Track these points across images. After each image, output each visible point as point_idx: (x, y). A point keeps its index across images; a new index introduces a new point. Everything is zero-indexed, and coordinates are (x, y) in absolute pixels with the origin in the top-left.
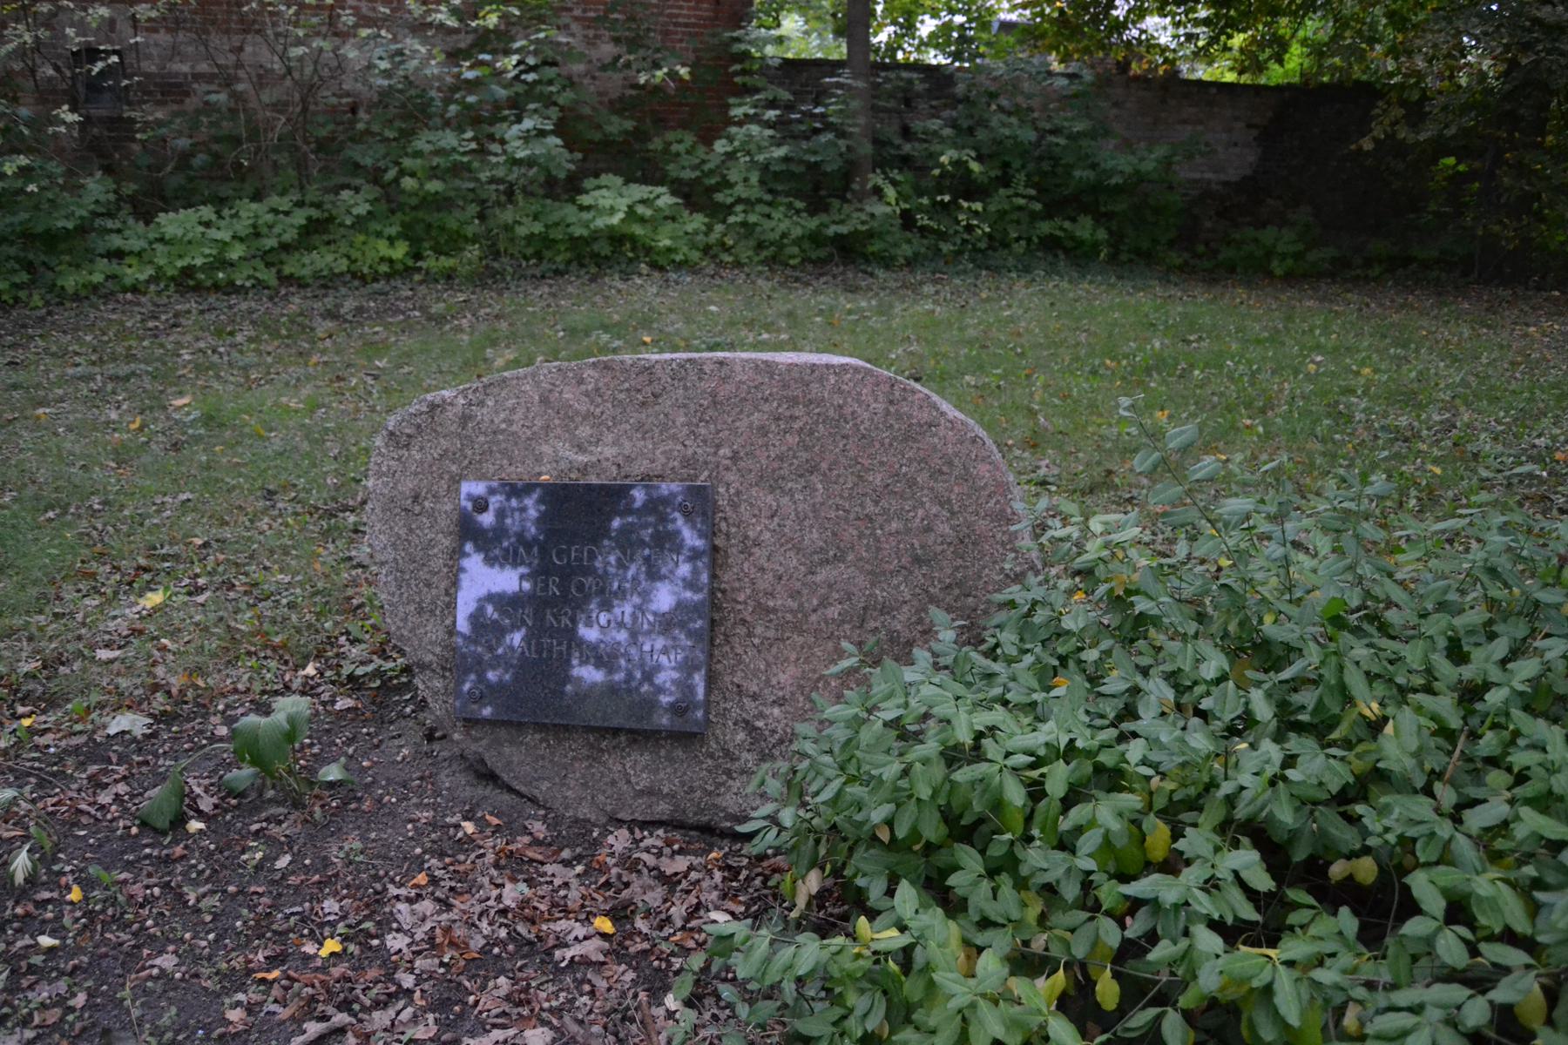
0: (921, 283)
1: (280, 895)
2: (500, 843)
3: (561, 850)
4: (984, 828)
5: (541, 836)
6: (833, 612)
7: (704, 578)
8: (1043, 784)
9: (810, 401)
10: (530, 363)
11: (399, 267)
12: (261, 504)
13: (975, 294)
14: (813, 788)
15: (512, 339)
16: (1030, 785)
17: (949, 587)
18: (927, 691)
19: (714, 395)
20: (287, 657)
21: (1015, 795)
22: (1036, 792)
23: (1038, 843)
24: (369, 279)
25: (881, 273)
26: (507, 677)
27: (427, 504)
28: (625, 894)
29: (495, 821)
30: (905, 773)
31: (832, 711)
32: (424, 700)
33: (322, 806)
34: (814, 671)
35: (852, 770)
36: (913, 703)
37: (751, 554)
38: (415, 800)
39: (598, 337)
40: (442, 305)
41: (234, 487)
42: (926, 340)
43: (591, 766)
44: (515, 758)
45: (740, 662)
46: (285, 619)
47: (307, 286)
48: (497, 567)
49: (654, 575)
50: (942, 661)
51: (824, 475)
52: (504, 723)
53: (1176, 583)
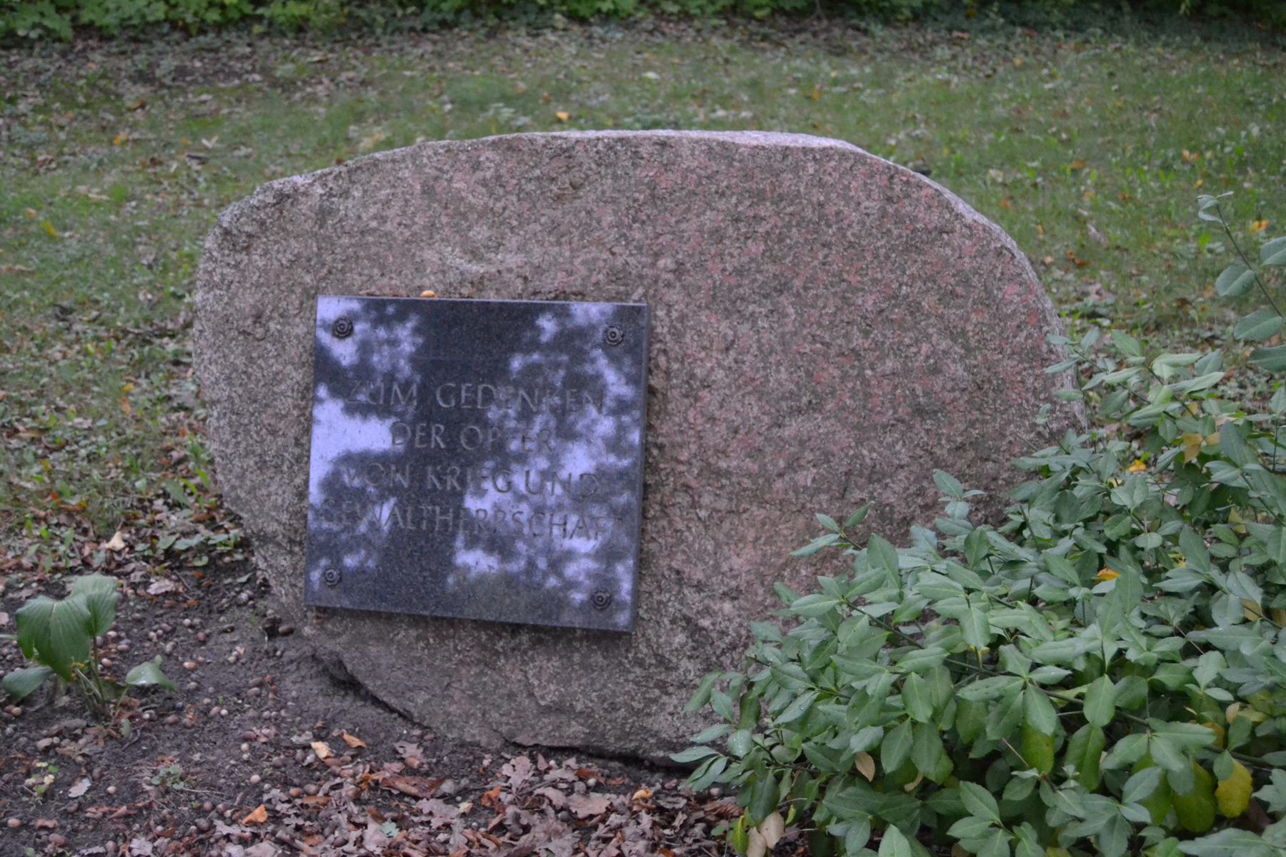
0: (934, 44)
1: (75, 831)
2: (362, 770)
3: (441, 781)
4: (1000, 765)
5: (416, 763)
6: (805, 477)
7: (635, 437)
8: (1080, 707)
9: (781, 198)
10: (408, 141)
11: (235, 15)
12: (52, 325)
13: (1006, 59)
14: (775, 706)
15: (382, 113)
16: (1062, 710)
17: (960, 448)
18: (929, 580)
19: (652, 186)
20: (86, 525)
21: (1044, 719)
22: (1072, 718)
23: (1072, 783)
24: (194, 32)
25: (878, 30)
26: (371, 564)
27: (272, 325)
28: (524, 840)
29: (356, 742)
30: (897, 688)
31: (803, 603)
32: (265, 583)
33: (131, 718)
34: (779, 555)
35: (826, 682)
36: (910, 595)
37: (697, 399)
38: (251, 713)
39: (497, 112)
40: (290, 66)
41: (16, 303)
42: (938, 121)
43: (482, 673)
44: (381, 659)
45: (682, 541)
46: (83, 476)
47: (111, 38)
48: (358, 416)
49: (567, 434)
50: (950, 544)
51: (798, 295)
52: (370, 614)
53: (1270, 448)
